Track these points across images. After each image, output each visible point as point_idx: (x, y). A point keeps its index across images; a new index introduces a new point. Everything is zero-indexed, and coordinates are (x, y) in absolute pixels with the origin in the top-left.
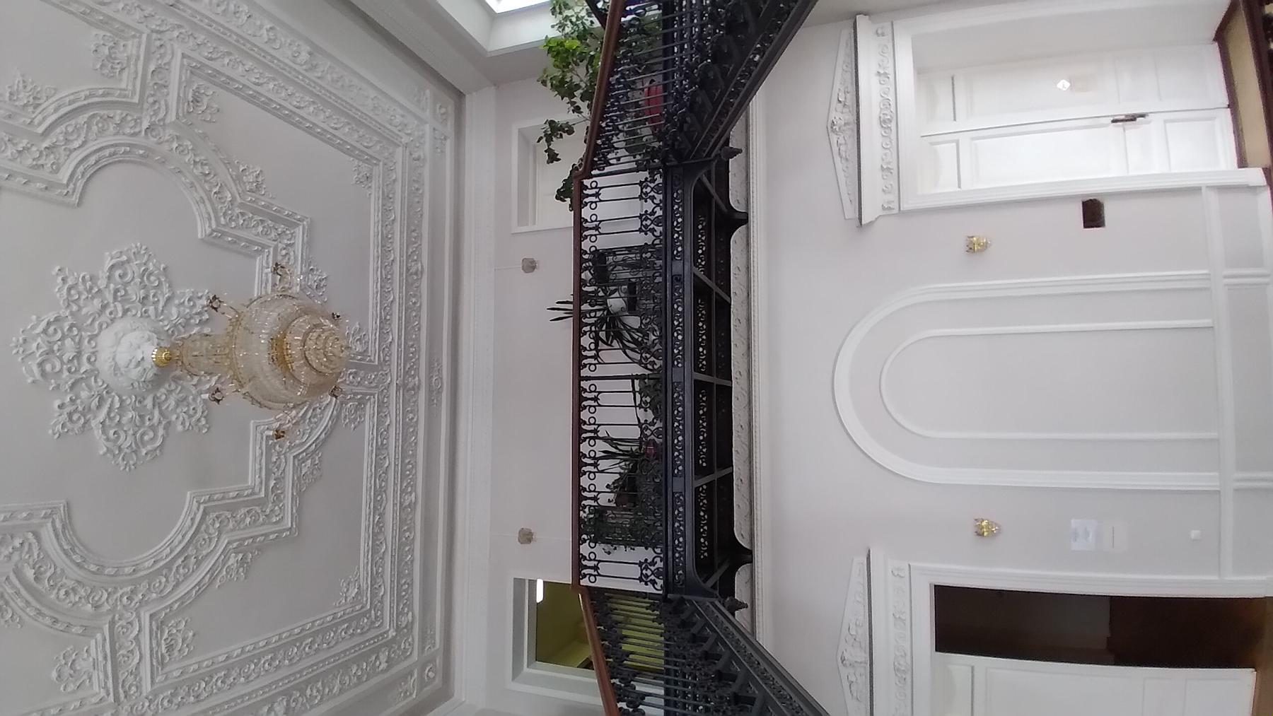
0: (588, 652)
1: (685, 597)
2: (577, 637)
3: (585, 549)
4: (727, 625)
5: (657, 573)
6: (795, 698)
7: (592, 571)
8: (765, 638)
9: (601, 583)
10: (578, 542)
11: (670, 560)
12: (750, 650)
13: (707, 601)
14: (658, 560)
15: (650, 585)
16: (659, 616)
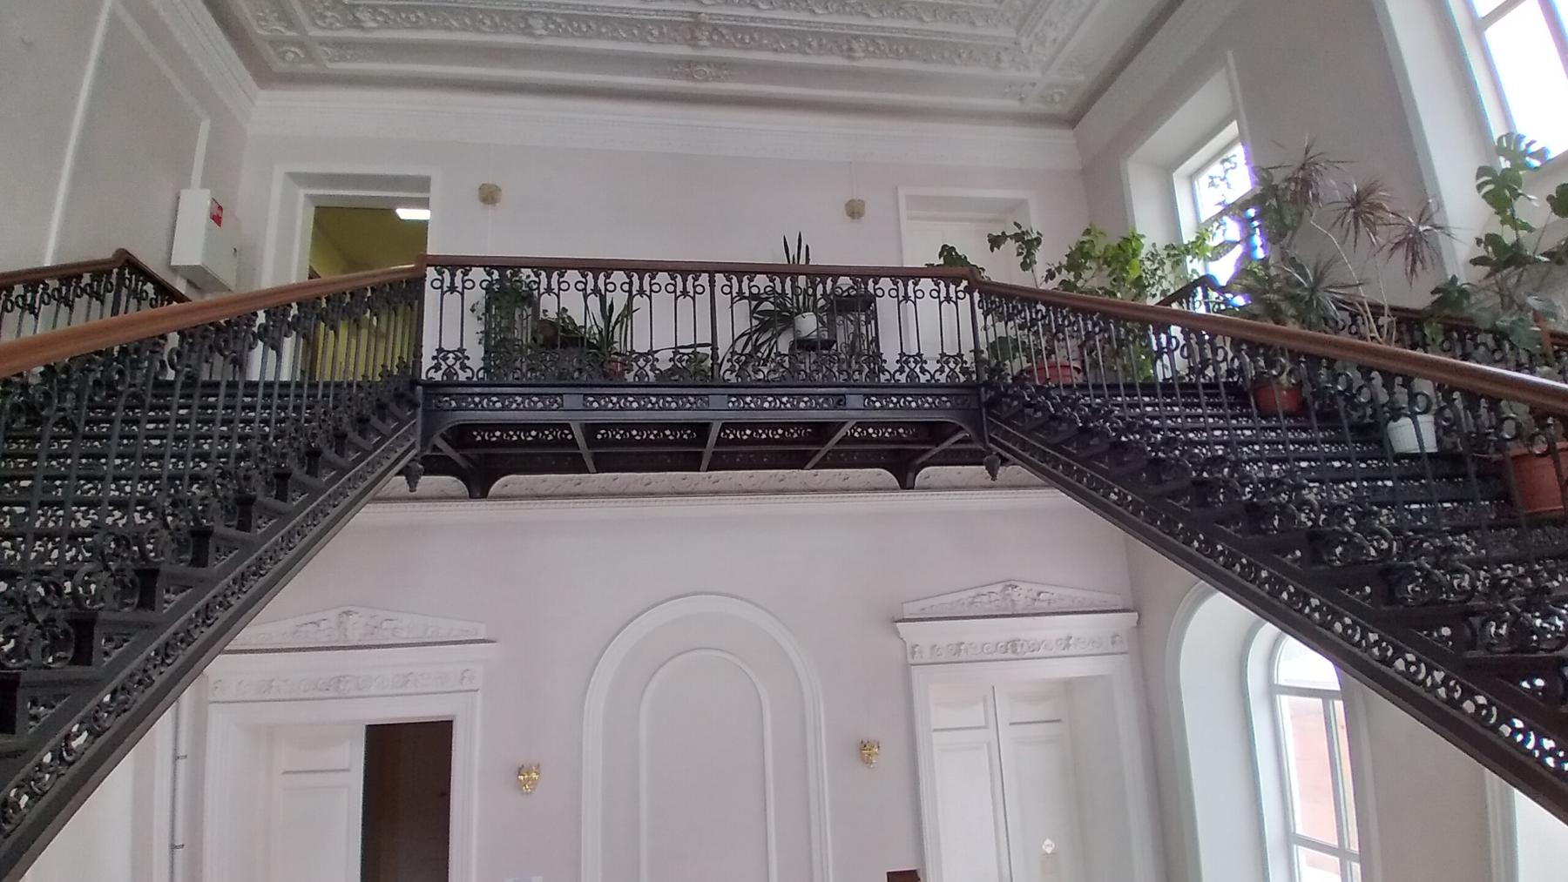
0: (326, 276)
1: (420, 410)
3: (478, 274)
5: (450, 372)
6: (291, 553)
8: (369, 515)
10: (489, 265)
11: (469, 390)
13: (416, 439)
16: (390, 374)
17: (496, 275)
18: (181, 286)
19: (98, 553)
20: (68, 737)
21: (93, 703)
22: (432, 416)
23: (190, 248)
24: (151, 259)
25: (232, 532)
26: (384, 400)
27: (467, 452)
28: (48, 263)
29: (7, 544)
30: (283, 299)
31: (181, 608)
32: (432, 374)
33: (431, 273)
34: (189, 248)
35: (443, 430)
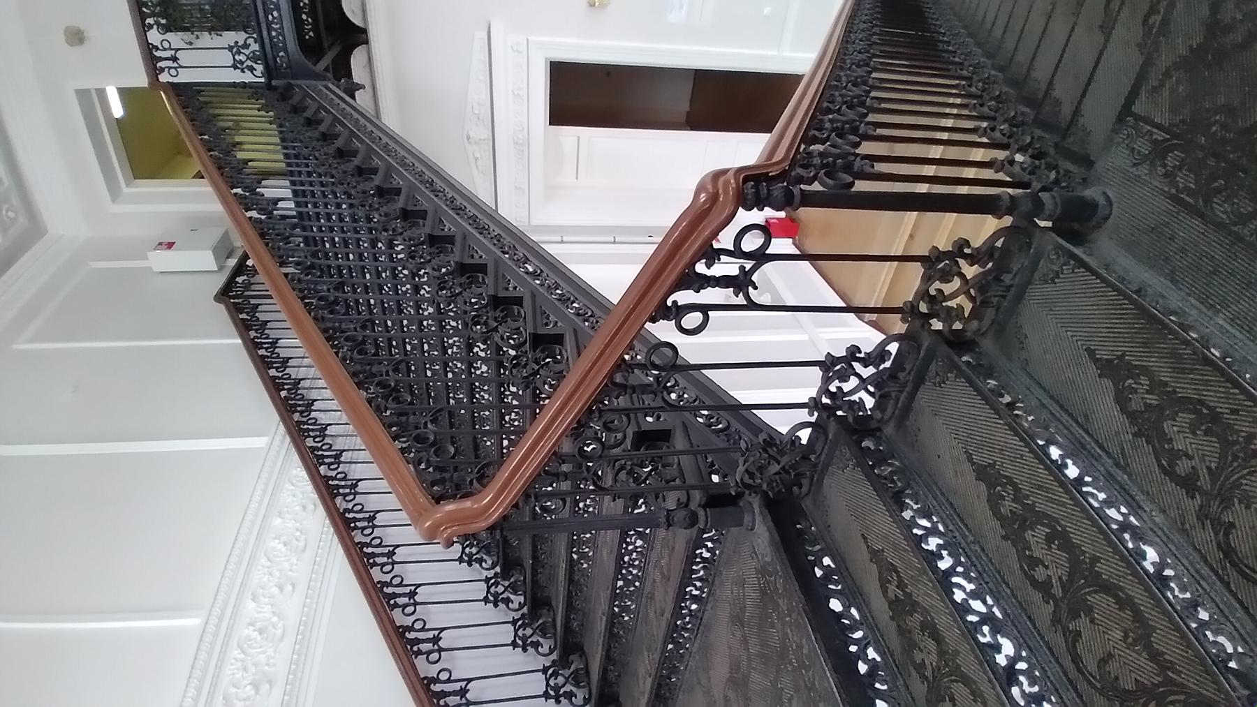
0: (197, 167)
1: (293, 82)
2: (180, 150)
3: (154, 36)
4: (344, 106)
5: (254, 58)
6: (417, 164)
7: (170, 63)
8: (391, 119)
9: (184, 77)
10: (143, 29)
11: (267, 41)
12: (370, 127)
13: (320, 85)
14: (250, 41)
15: (248, 72)
16: (263, 105)
17: (150, 21)
18: (232, 262)
19: (453, 298)
20: (527, 273)
21: (510, 263)
22: (297, 72)
23: (204, 260)
24: (220, 281)
25: (457, 249)
26: (302, 120)
27: (326, 44)
28: (239, 341)
29: (450, 351)
30: (231, 199)
31: (454, 222)
32: (258, 73)
33: (164, 78)
34: (201, 263)
35: (310, 64)
